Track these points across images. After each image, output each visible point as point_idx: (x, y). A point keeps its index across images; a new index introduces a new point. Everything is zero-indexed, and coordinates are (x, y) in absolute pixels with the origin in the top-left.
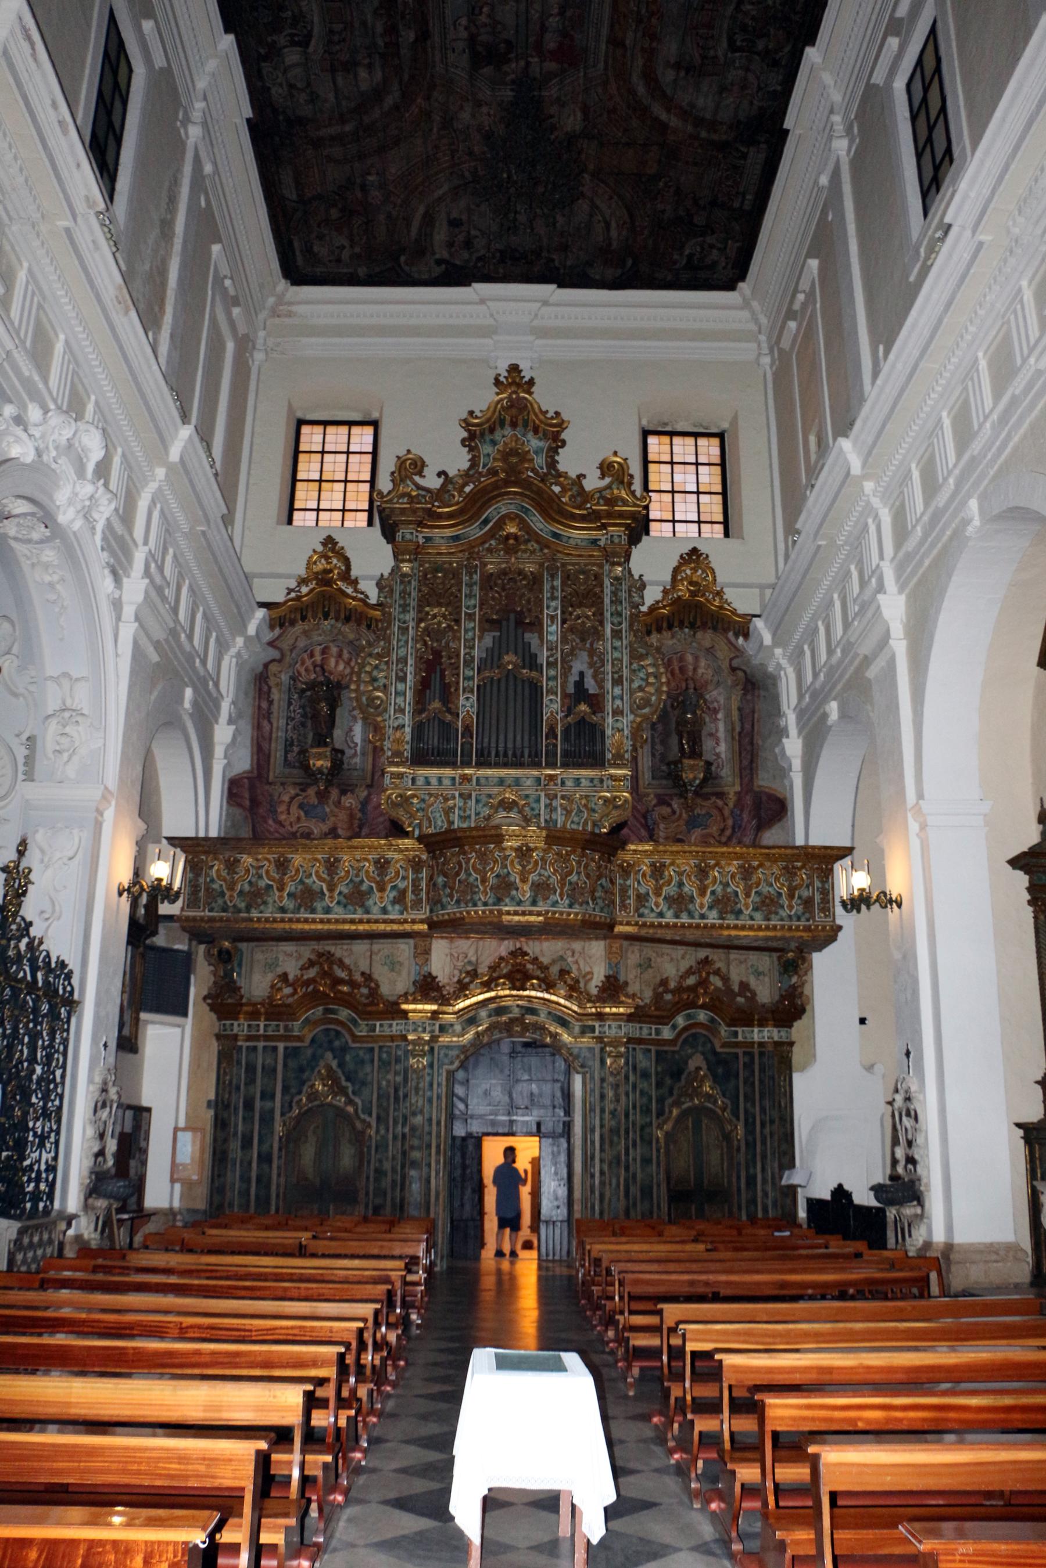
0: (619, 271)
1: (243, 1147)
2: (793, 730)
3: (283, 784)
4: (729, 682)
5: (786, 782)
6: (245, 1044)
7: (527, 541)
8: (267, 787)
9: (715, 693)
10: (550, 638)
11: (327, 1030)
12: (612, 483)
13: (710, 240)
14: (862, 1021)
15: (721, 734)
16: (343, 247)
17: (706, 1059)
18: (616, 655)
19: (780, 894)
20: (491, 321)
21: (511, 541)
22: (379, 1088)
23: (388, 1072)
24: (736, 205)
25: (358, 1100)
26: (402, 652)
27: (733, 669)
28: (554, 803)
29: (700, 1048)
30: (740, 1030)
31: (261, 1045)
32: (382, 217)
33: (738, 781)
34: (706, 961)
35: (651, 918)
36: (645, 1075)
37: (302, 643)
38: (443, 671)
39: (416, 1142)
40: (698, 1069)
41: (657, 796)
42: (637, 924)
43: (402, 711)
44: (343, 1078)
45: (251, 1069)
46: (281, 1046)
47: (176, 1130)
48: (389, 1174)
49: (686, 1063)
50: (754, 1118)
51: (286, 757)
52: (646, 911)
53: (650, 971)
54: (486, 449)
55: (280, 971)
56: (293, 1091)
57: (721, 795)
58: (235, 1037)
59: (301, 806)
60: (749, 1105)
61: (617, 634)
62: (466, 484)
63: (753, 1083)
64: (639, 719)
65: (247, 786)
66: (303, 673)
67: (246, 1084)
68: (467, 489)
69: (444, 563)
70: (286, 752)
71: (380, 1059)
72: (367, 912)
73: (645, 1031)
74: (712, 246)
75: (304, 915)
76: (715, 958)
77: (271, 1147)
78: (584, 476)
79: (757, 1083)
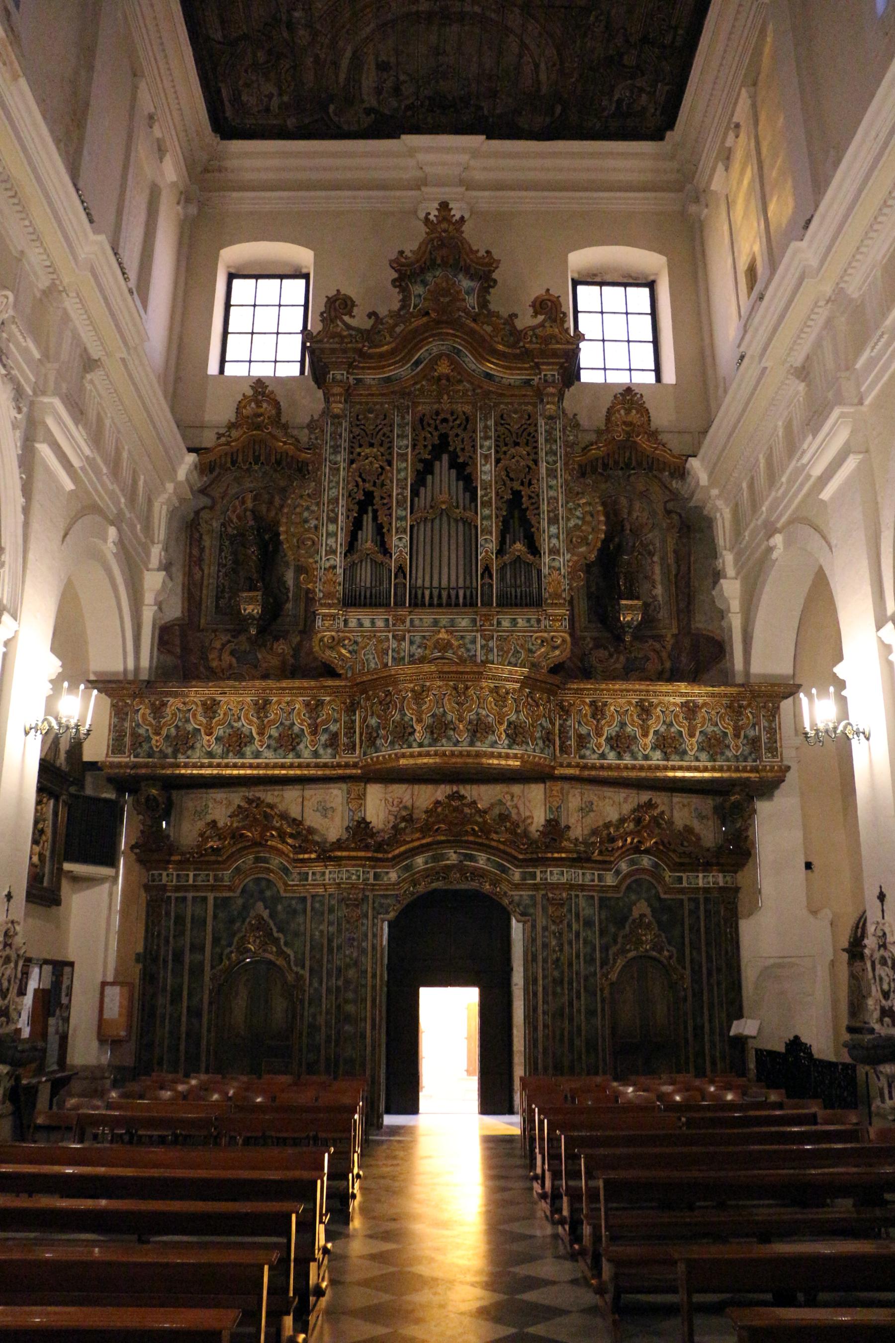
0: (548, 120)
1: (172, 1002)
2: (730, 571)
3: (215, 631)
4: (665, 525)
5: (724, 624)
6: (174, 895)
7: (460, 382)
8: (198, 634)
9: (650, 535)
10: (484, 477)
11: (258, 879)
12: (544, 321)
13: (639, 83)
14: (808, 866)
15: (658, 577)
16: (270, 96)
17: (650, 905)
18: (552, 493)
19: (725, 734)
20: (419, 174)
21: (444, 382)
22: (312, 940)
23: (321, 922)
24: (667, 40)
25: (289, 951)
26: (333, 493)
27: (668, 512)
28: (491, 644)
29: (644, 895)
30: (684, 876)
31: (190, 895)
32: (309, 61)
33: (675, 623)
34: (650, 805)
35: (593, 760)
36: (588, 924)
37: (233, 491)
38: (375, 512)
39: (350, 995)
40: (642, 916)
41: (594, 639)
42: (578, 765)
43: (334, 552)
44: (275, 930)
45: (180, 920)
46: (211, 896)
47: (104, 984)
48: (323, 1028)
49: (630, 910)
50: (701, 967)
51: (217, 606)
52: (588, 753)
53: (592, 814)
54: (418, 289)
55: (209, 818)
56: (223, 942)
57: (659, 638)
58: (164, 888)
59: (232, 653)
60: (695, 954)
61: (552, 473)
62: (396, 325)
63: (698, 930)
64: (575, 558)
65: (178, 633)
66: (235, 520)
67: (174, 937)
68: (398, 330)
69: (375, 404)
70: (218, 598)
71: (313, 909)
72: (299, 756)
73: (588, 877)
74: (641, 90)
75: (232, 760)
76: (659, 801)
77: (201, 1000)
78: (516, 316)
79: (702, 930)
